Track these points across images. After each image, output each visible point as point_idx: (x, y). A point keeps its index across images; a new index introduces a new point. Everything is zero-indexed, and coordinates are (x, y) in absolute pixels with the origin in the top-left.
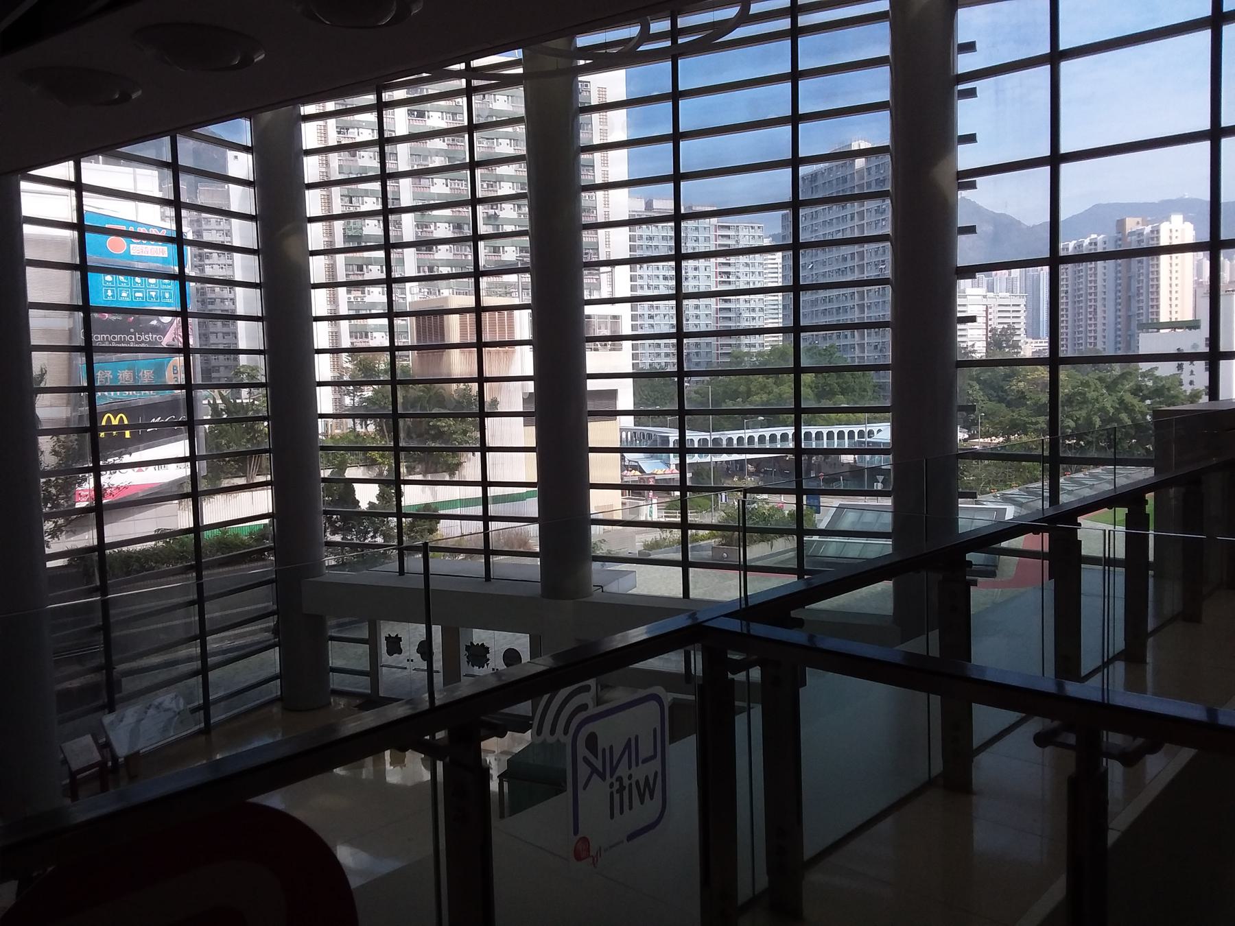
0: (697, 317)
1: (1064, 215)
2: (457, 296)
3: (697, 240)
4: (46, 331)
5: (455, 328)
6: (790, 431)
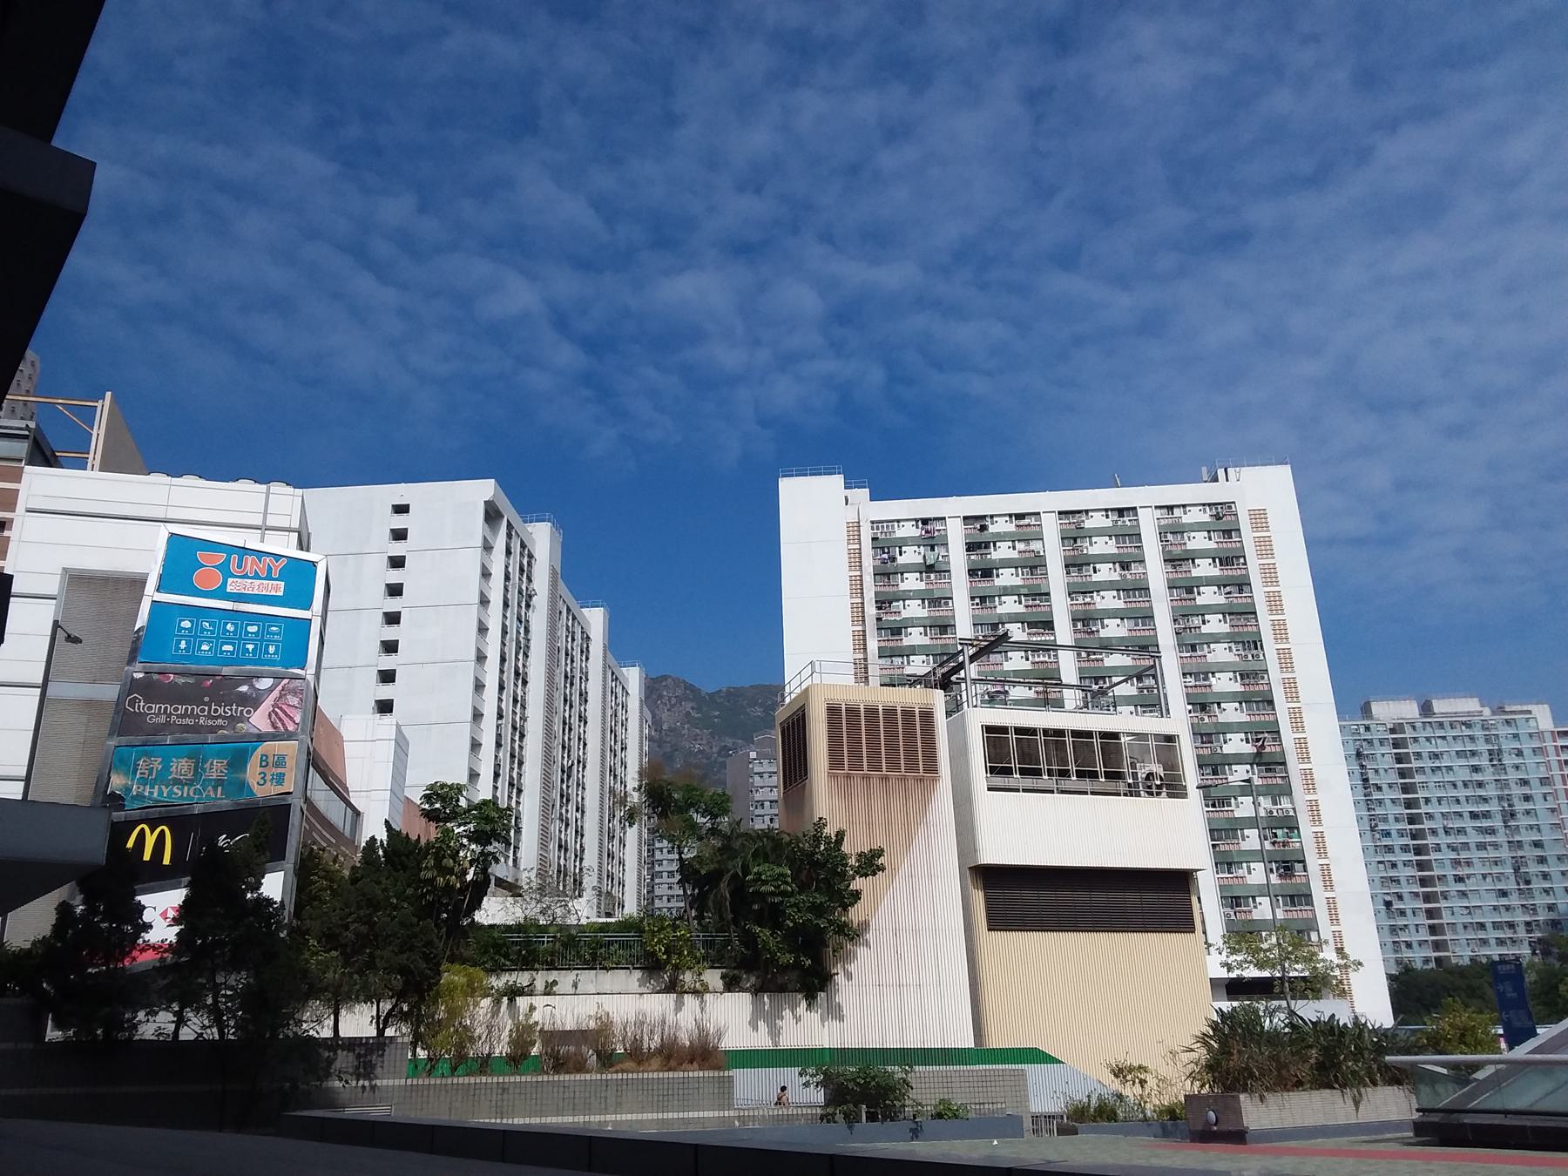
0: (1545, 876)
3: (1520, 753)
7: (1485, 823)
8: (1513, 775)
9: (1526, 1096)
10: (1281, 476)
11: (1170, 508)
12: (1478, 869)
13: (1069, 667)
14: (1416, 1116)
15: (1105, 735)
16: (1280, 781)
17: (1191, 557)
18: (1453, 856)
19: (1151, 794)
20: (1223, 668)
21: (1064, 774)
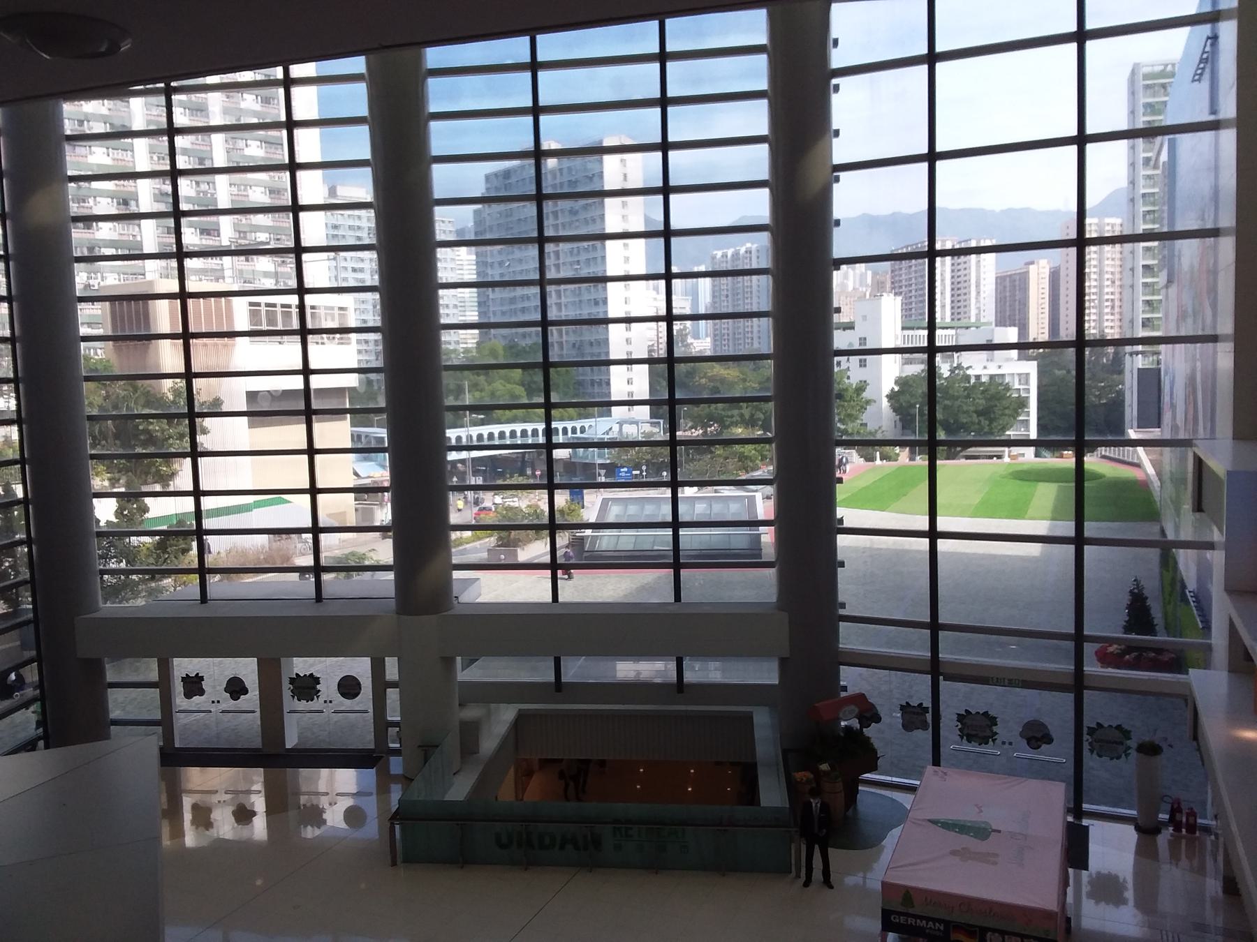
1: (1090, 203)
2: (159, 276)
4: (872, 223)
5: (164, 316)
6: (541, 427)
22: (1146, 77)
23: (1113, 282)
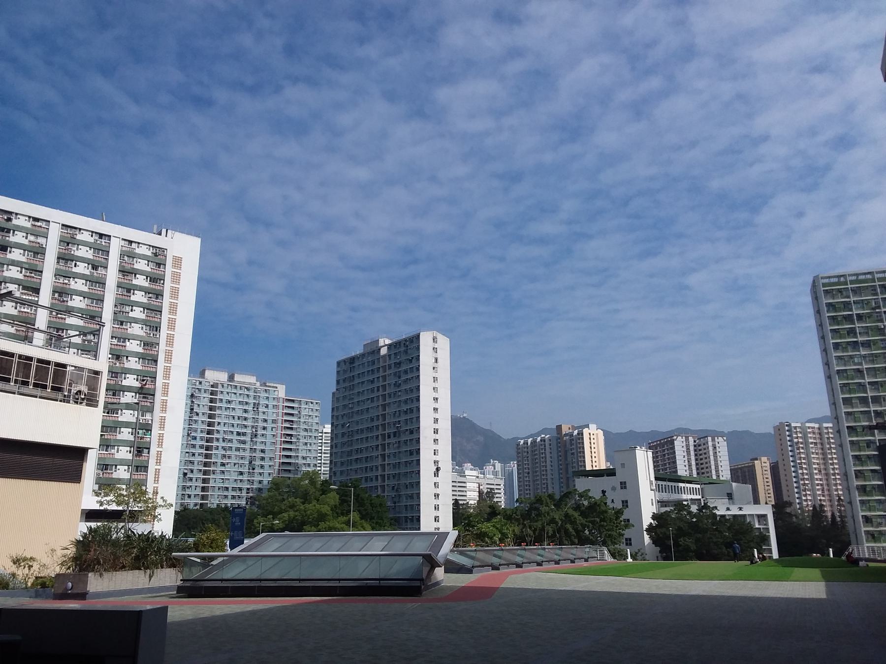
0: (262, 467)
3: (267, 406)
7: (242, 438)
8: (261, 417)
9: (232, 573)
10: (194, 243)
11: (131, 242)
12: (233, 461)
13: (42, 319)
14: (179, 583)
15: (58, 365)
16: (149, 404)
17: (135, 273)
18: (223, 452)
19: (77, 403)
20: (135, 337)
21: (25, 383)
22: (824, 285)
23: (820, 471)
